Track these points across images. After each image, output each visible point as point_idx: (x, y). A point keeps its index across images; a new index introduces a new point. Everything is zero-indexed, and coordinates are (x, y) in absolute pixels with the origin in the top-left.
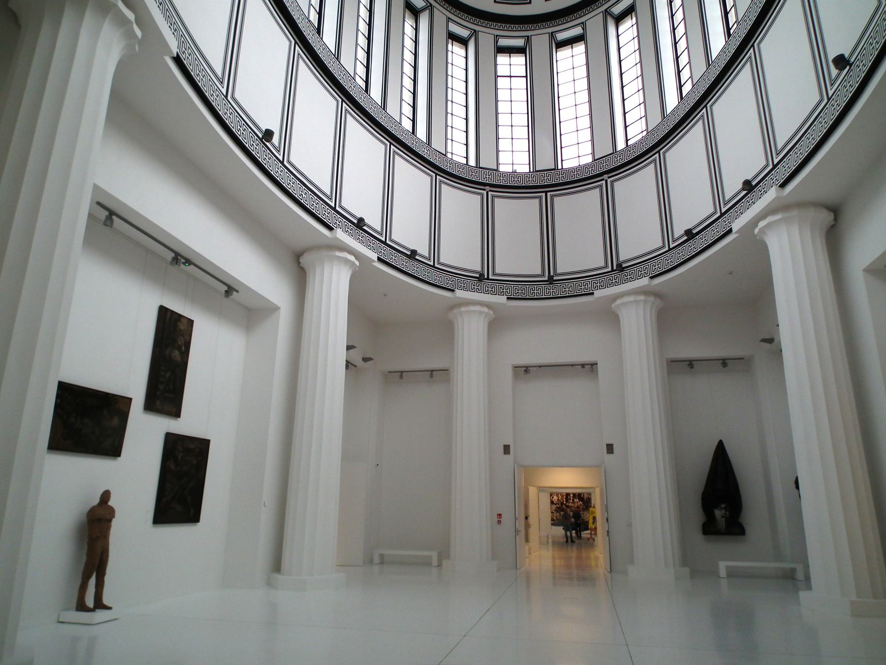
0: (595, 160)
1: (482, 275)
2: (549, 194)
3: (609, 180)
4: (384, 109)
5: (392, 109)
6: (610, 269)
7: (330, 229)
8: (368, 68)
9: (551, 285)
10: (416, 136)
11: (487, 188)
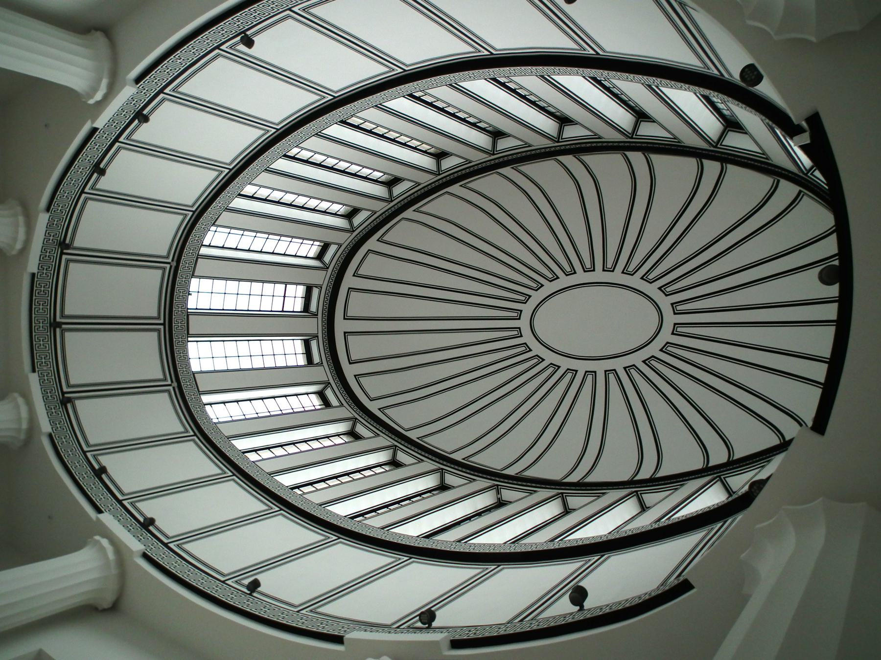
1: (68, 247)
2: (162, 327)
3: (171, 388)
4: (266, 170)
5: (265, 178)
6: (65, 389)
7: (138, 80)
8: (306, 162)
9: (48, 325)
10: (236, 197)
11: (174, 264)
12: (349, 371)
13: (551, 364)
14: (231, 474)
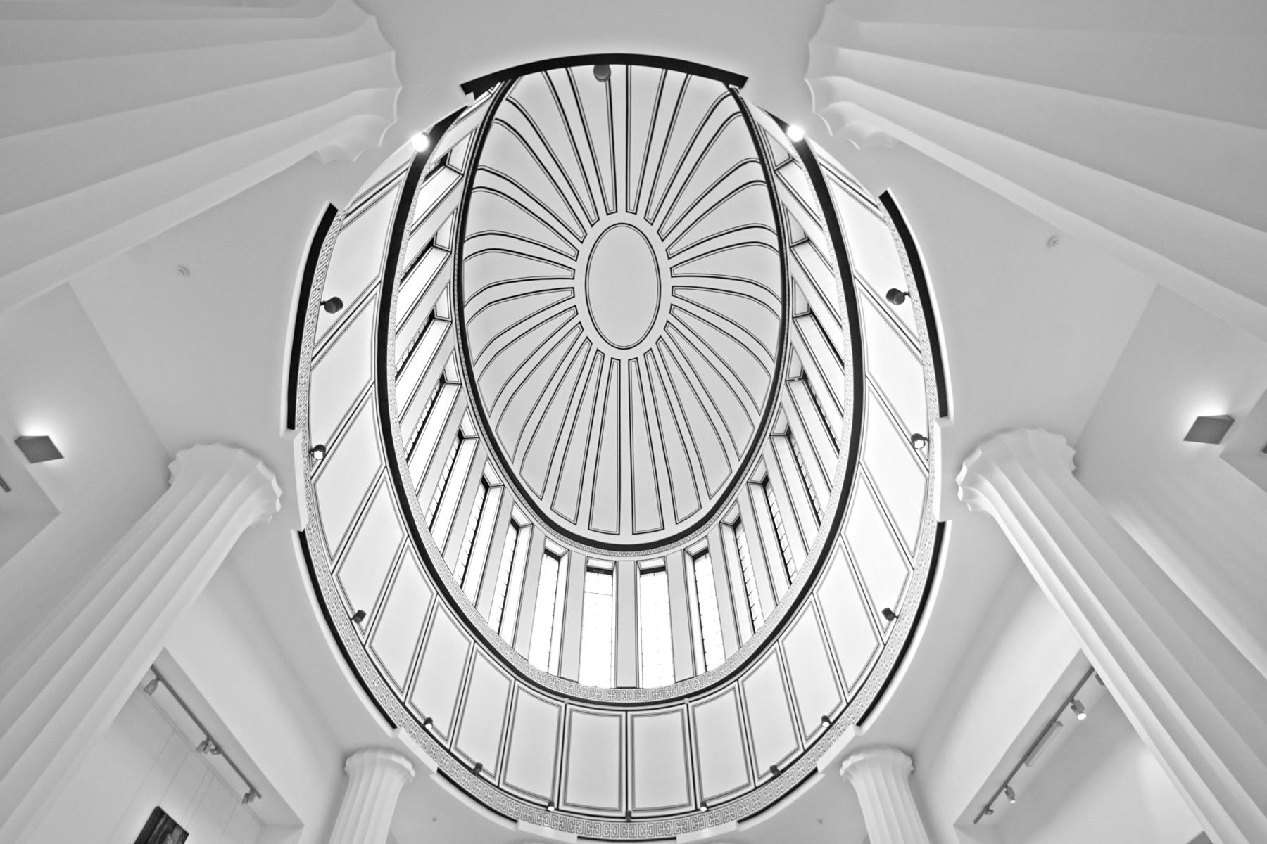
0: (676, 682)
2: (629, 713)
3: (690, 705)
4: (475, 607)
6: (693, 808)
7: (394, 726)
11: (567, 700)
12: (672, 530)
13: (664, 329)
14: (777, 643)
